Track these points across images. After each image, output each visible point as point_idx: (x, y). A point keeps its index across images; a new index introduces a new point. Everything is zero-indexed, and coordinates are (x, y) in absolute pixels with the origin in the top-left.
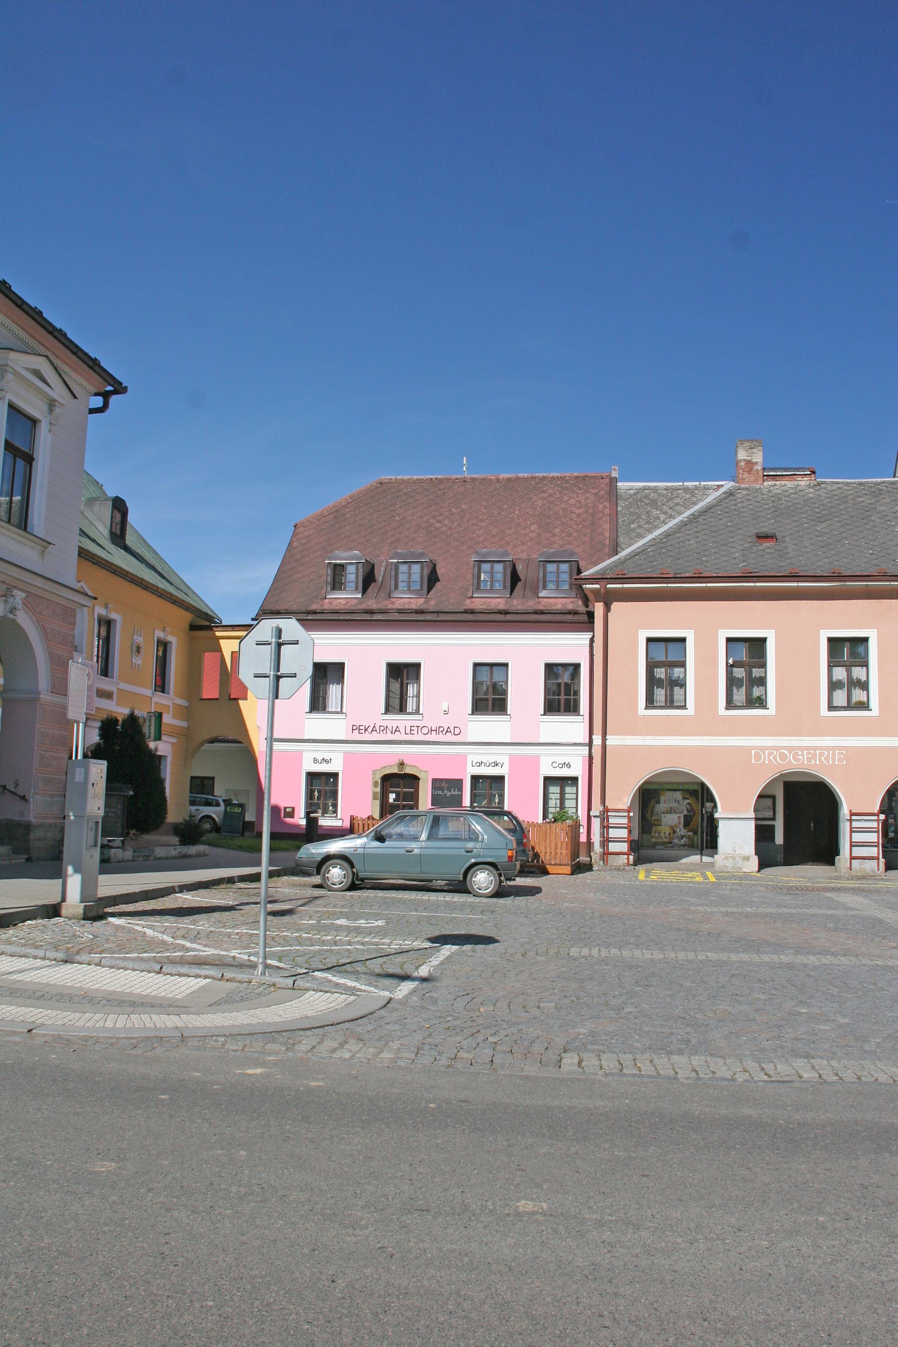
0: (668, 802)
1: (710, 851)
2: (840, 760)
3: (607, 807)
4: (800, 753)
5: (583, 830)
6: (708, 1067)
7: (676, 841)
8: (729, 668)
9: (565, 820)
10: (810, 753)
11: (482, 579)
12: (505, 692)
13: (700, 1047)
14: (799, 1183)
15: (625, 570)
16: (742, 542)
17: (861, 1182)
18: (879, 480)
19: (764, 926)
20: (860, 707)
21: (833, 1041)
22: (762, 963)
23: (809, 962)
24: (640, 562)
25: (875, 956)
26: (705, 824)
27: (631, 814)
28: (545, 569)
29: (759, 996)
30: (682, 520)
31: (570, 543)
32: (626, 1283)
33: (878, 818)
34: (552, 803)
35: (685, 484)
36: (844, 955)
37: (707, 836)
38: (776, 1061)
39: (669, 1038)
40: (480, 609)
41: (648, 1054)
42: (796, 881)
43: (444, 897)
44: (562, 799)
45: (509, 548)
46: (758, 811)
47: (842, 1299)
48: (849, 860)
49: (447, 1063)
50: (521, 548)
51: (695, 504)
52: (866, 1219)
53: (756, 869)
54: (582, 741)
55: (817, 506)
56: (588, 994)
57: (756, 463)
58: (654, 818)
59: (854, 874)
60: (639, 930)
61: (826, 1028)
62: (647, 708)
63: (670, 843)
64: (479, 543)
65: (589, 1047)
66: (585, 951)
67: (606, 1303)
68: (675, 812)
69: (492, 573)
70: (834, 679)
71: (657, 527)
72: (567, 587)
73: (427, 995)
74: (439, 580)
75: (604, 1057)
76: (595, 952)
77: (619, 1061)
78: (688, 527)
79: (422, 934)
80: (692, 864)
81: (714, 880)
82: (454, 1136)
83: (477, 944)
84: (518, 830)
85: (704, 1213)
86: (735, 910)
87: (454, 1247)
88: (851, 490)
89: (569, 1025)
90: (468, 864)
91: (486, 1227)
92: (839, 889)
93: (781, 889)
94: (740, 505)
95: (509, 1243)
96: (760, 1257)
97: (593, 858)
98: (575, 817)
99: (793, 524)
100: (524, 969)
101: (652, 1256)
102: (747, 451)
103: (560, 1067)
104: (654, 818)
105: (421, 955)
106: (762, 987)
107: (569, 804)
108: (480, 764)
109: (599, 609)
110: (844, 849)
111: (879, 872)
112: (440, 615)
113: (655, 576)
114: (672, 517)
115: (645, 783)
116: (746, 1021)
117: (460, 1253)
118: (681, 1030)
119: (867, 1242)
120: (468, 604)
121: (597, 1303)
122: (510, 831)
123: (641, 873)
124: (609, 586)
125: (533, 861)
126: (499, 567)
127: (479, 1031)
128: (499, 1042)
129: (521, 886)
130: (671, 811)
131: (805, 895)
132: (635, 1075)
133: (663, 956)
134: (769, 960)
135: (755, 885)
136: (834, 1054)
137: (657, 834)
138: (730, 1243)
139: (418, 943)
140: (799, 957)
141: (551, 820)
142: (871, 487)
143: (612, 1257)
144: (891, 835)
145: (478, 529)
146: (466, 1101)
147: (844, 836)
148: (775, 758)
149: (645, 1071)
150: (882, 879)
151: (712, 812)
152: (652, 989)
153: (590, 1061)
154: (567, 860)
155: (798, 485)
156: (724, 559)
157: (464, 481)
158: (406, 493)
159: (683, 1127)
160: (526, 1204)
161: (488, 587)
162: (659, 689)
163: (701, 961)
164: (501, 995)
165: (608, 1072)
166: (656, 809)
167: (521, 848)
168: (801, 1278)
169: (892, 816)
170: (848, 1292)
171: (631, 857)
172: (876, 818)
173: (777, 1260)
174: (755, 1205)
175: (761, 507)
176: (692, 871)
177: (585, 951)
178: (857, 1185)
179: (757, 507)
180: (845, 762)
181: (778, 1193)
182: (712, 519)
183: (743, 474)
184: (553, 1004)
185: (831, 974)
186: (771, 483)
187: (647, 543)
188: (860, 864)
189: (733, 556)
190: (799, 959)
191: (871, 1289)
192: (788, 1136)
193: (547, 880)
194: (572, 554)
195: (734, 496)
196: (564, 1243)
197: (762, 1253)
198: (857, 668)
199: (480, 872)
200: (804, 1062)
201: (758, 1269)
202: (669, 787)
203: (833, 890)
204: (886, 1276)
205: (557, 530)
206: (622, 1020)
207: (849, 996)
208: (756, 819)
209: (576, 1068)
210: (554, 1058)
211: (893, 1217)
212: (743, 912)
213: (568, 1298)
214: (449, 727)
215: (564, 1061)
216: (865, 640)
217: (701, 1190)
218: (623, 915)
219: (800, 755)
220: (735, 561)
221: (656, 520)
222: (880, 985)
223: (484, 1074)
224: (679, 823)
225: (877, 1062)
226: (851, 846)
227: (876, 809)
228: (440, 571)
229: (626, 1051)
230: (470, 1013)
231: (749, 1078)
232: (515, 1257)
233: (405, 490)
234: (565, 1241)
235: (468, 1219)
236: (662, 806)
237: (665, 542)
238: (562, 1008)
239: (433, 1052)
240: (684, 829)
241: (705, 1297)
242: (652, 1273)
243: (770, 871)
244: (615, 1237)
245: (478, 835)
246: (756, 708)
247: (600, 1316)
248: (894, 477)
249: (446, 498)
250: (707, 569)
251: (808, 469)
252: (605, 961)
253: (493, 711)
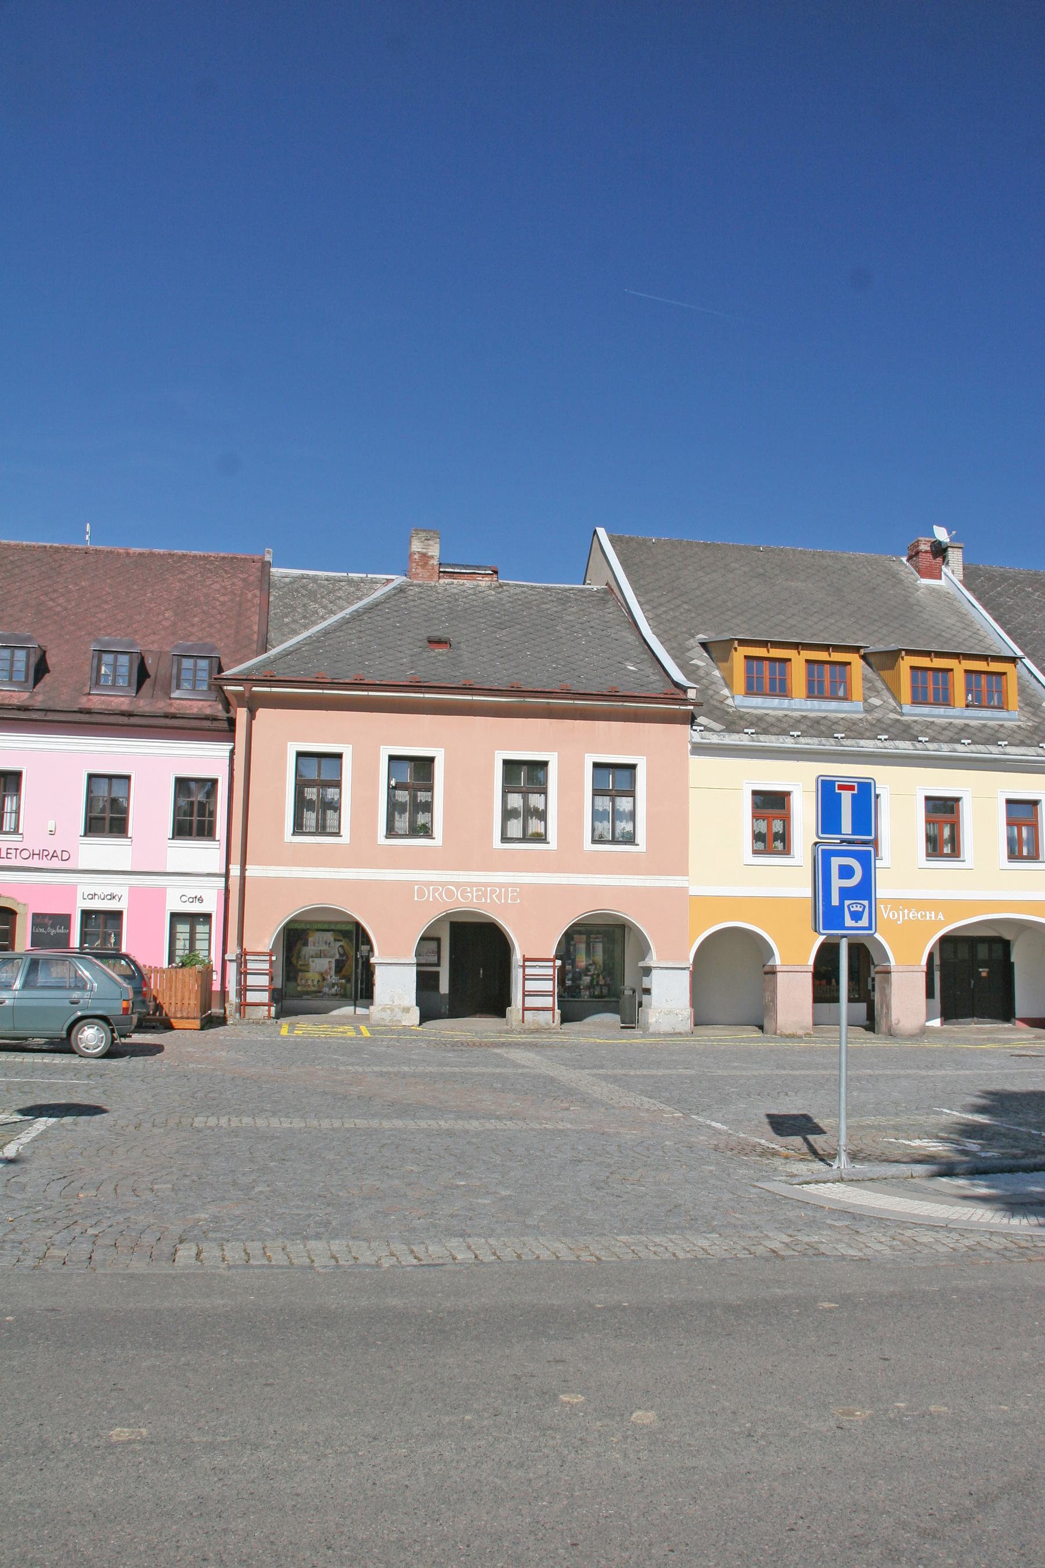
0: (317, 945)
1: (364, 1001)
2: (513, 899)
3: (245, 949)
5: (216, 977)
6: (350, 1252)
7: (326, 990)
8: (390, 790)
9: (195, 964)
11: (103, 672)
12: (126, 811)
13: (341, 1230)
14: (446, 1380)
15: (275, 671)
16: (411, 647)
17: (514, 1373)
18: (567, 586)
19: (423, 1087)
20: (537, 839)
21: (493, 1216)
22: (418, 1129)
23: (472, 1128)
24: (292, 663)
25: (545, 1118)
26: (359, 971)
27: (274, 958)
28: (179, 664)
29: (412, 1168)
30: (344, 617)
31: (211, 635)
32: (239, 1515)
33: (554, 964)
34: (179, 944)
35: (350, 574)
36: (511, 1119)
37: (361, 984)
38: (427, 1242)
39: (306, 1220)
40: (100, 709)
41: (280, 1240)
42: (461, 1035)
43: (43, 1059)
44: (192, 940)
45: (137, 637)
46: (420, 955)
47: (484, 1504)
48: (521, 1011)
49: (33, 1264)
50: (152, 638)
51: (360, 599)
52: (517, 1412)
53: (418, 1022)
54: (217, 871)
55: (497, 610)
56: (212, 1172)
57: (432, 557)
58: (300, 963)
59: (527, 1027)
60: (277, 1095)
61: (486, 1201)
62: (294, 833)
63: (320, 992)
64: (100, 630)
65: (210, 1235)
66: (212, 1121)
67: (212, 1543)
68: (325, 956)
69: (115, 667)
70: (509, 807)
71: (314, 623)
72: (205, 688)
73: (13, 1180)
74: (49, 671)
75: (228, 1247)
76: (224, 1121)
77: (245, 1250)
78: (350, 625)
79: (11, 1104)
80: (344, 1016)
81: (368, 1035)
82: (35, 1355)
83: (80, 1115)
84: (137, 977)
85: (335, 1423)
86: (391, 1069)
87: (23, 1497)
88: (536, 595)
89: (187, 1210)
90: (73, 1018)
91: (67, 1466)
92: (510, 1044)
93: (445, 1044)
94: (412, 603)
95: (96, 1483)
96: (396, 1467)
97: (228, 1010)
98: (207, 961)
99: (469, 629)
100: (136, 1144)
101: (272, 1479)
102: (422, 542)
103: (174, 1261)
104: (300, 963)
105: (8, 1131)
106: (417, 1157)
107: (199, 945)
108: (93, 896)
109: (241, 715)
110: (516, 998)
111: (554, 1025)
112: (49, 713)
113: (309, 680)
114: (332, 612)
115: (291, 921)
116: (396, 1197)
117: (31, 1505)
118: (320, 1211)
119: (516, 1438)
120: (84, 702)
121: (202, 1545)
122: (126, 977)
123: (284, 1027)
124: (254, 689)
125: (154, 1014)
126: (124, 660)
127: (76, 1222)
128: (100, 1235)
129: (139, 1044)
130: (320, 955)
131: (471, 1051)
132: (263, 1266)
133: (304, 1125)
134: (426, 1126)
135: (415, 1040)
136: (493, 1230)
137: (304, 982)
138: (364, 1454)
139: (6, 1116)
140: (460, 1122)
141: (178, 964)
142: (559, 593)
143: (223, 1485)
144: (569, 983)
145: (100, 612)
146: (53, 1310)
147: (516, 984)
148: (440, 895)
149: (276, 1260)
150: (558, 1033)
151: (369, 956)
152: (288, 1164)
153: (211, 1252)
154: (196, 1013)
155: (478, 586)
156: (390, 664)
157: (86, 553)
158: (12, 562)
159: (317, 1324)
160: (121, 1432)
161: (110, 683)
162: (309, 812)
163: (348, 1130)
164: (105, 1177)
165: (231, 1264)
166: (303, 952)
167: (140, 998)
168: (442, 1486)
169: (570, 961)
170: (492, 1496)
171: (273, 1009)
172: (551, 964)
173: (416, 1470)
174: (395, 1408)
175: (435, 607)
176: (344, 1024)
177: (212, 1121)
178: (510, 1376)
179: (431, 607)
180: (519, 901)
181: (422, 1392)
182: (379, 618)
183: (417, 568)
184: (170, 1186)
185: (494, 1140)
186: (447, 581)
187: (302, 640)
189: (401, 661)
190: (460, 1125)
191: (516, 1489)
192: (437, 1327)
193: (171, 1036)
194: (214, 649)
195: (405, 592)
196: (166, 1475)
197: (400, 1463)
198: (534, 795)
199: (88, 1028)
200: (459, 1242)
201: (395, 1482)
202: (320, 926)
203: (503, 1045)
204: (534, 1474)
205: (196, 619)
206: (251, 1202)
207: (514, 1165)
208: (418, 965)
209: (193, 1261)
210: (167, 1250)
211: (546, 1408)
212: (399, 1072)
213: (166, 1544)
214: (55, 851)
215: (179, 1253)
216: (545, 764)
217: (333, 1396)
218: (260, 1077)
219: (468, 892)
220: (403, 668)
221: (313, 615)
222: (547, 1151)
223: (79, 1275)
224: (330, 969)
225: (540, 1238)
226: (524, 995)
227: (552, 954)
228: (51, 660)
229: (254, 1239)
230: (66, 1200)
231: (397, 1264)
232: (103, 1500)
233: (11, 558)
234: (167, 1472)
235: (45, 1459)
236: (310, 949)
237: (323, 641)
238: (180, 1190)
239: (16, 1252)
240: (336, 976)
241: (331, 1521)
242: (270, 1500)
243: (432, 1025)
244: (228, 1461)
245: (86, 984)
246: (421, 837)
247: (205, 1560)
248: (584, 584)
249: (63, 571)
250: (370, 675)
251: (490, 568)
252: (235, 1132)
253: (110, 833)
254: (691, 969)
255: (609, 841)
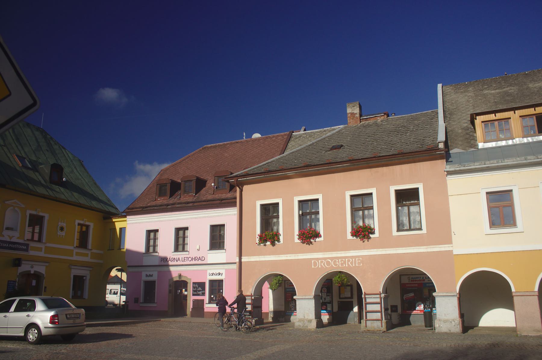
4: (337, 261)
10: (343, 260)
33: (380, 296)
57: (356, 114)
111: (382, 328)
148: (324, 264)
172: (378, 296)
180: (361, 265)
188: (371, 324)
219: (337, 262)
254: (458, 296)
255: (408, 230)
